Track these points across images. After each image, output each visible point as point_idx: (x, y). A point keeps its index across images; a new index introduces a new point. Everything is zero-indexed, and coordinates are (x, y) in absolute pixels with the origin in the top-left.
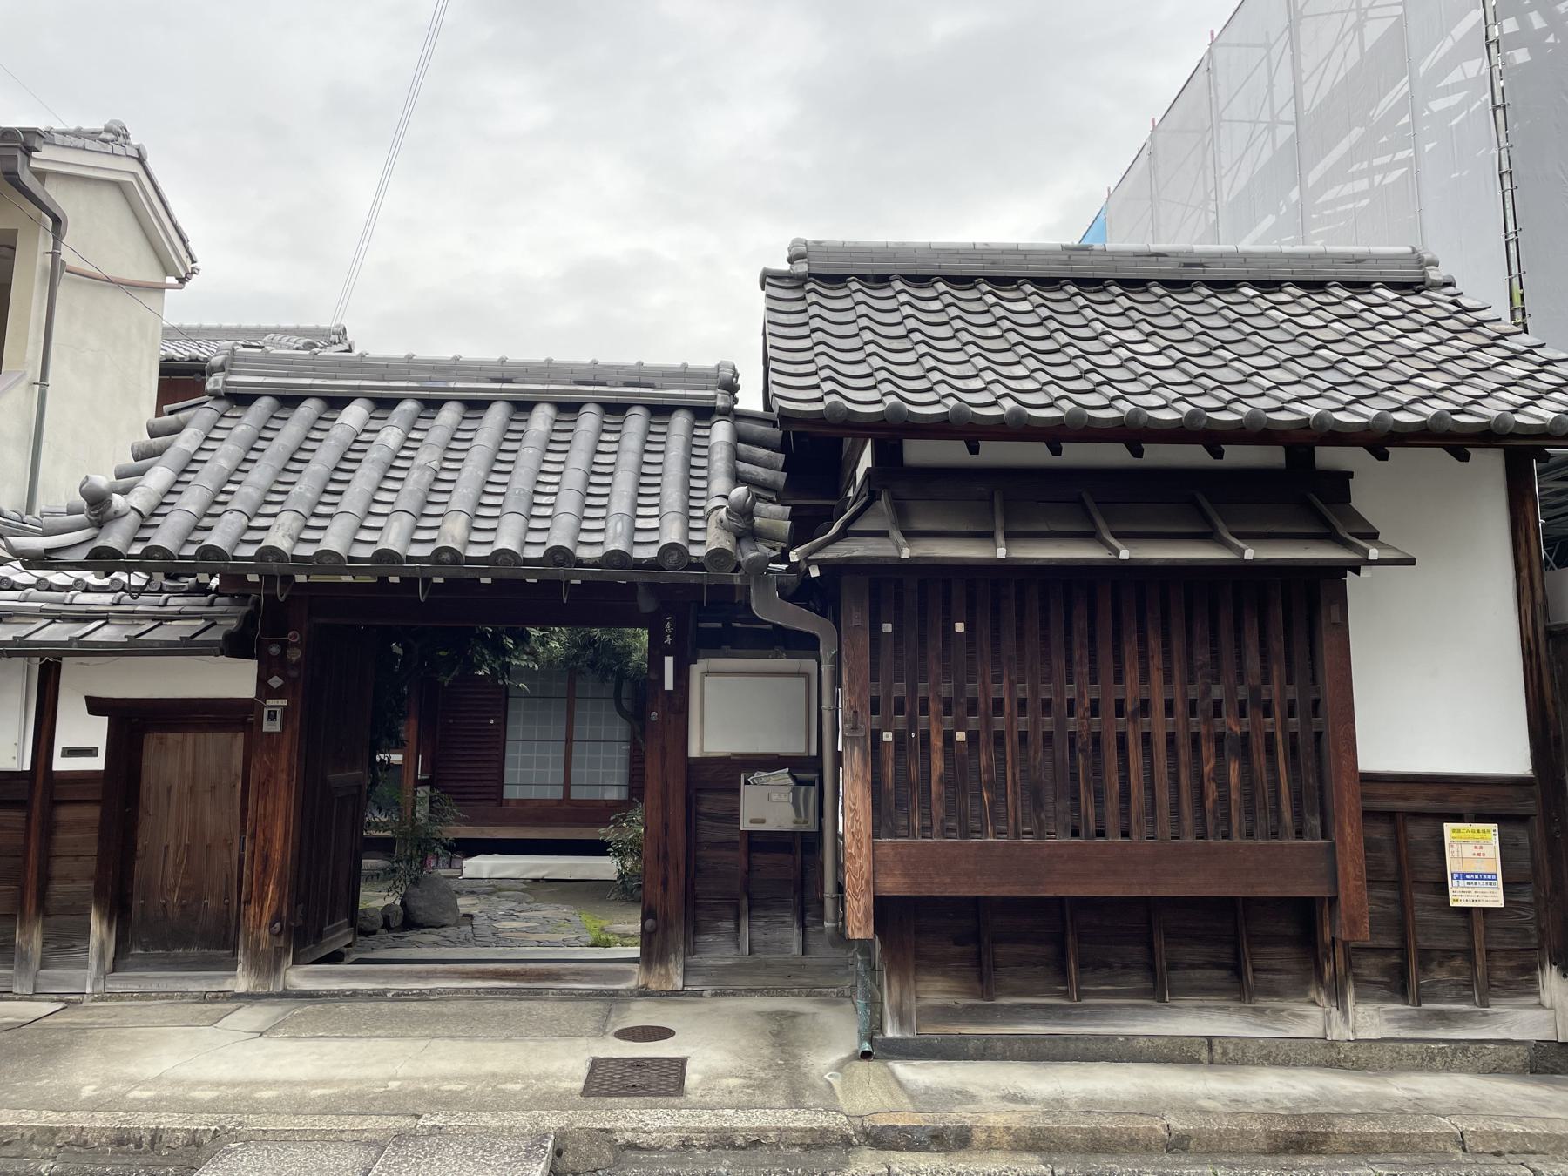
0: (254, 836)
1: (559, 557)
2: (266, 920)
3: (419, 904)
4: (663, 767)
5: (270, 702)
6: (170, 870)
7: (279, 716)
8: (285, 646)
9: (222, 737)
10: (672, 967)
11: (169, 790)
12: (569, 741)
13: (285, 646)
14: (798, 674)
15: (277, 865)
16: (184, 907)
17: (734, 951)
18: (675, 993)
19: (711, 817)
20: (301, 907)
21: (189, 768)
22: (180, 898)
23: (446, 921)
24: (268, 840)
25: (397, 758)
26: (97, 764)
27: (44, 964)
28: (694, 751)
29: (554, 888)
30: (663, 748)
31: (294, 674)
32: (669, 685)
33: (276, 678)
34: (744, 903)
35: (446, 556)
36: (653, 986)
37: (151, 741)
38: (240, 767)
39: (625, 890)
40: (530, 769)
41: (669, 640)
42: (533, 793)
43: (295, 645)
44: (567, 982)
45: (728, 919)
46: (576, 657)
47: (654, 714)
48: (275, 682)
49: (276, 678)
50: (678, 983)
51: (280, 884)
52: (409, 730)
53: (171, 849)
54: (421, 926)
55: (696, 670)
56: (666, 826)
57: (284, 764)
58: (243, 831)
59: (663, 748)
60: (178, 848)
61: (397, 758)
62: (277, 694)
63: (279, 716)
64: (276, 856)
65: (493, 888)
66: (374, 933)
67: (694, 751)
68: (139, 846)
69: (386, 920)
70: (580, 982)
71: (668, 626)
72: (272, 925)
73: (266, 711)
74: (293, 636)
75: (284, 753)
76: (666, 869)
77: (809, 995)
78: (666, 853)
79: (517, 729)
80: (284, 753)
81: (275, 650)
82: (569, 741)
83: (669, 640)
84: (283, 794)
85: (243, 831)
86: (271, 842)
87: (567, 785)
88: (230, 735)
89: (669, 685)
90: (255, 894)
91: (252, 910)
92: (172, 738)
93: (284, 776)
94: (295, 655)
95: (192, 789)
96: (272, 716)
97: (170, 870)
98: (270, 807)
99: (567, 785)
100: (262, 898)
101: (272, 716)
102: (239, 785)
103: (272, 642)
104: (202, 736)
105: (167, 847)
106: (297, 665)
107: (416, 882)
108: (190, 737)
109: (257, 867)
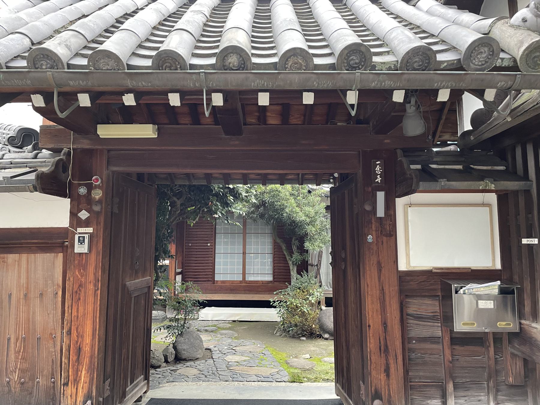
0: (69, 332)
1: (355, 59)
3: (185, 348)
4: (379, 278)
5: (80, 230)
6: (12, 356)
7: (86, 241)
8: (90, 188)
11: (10, 296)
12: (244, 253)
13: (90, 188)
14: (483, 205)
15: (88, 355)
16: (22, 384)
19: (419, 318)
20: (107, 382)
21: (23, 280)
22: (20, 378)
23: (198, 356)
24: (80, 336)
25: (167, 262)
27: (397, 61)
28: (402, 266)
29: (246, 326)
31: (97, 208)
32: (381, 212)
34: (450, 387)
35: (233, 60)
38: (61, 279)
39: (285, 330)
40: (227, 265)
41: (379, 179)
42: (228, 278)
43: (98, 187)
45: (435, 398)
46: (253, 212)
48: (84, 215)
51: (90, 369)
52: (172, 248)
53: (13, 340)
54: (185, 360)
55: (400, 202)
56: (385, 324)
57: (91, 277)
58: (63, 328)
60: (17, 340)
61: (167, 262)
62: (86, 223)
63: (86, 241)
64: (86, 349)
65: (215, 328)
66: (159, 367)
67: (402, 266)
69: (166, 357)
73: (77, 237)
74: (97, 181)
75: (91, 269)
78: (386, 346)
79: (220, 248)
80: (91, 269)
81: (83, 191)
82: (244, 253)
83: (379, 179)
84: (91, 299)
85: (63, 328)
86: (82, 337)
87: (244, 274)
89: (381, 212)
91: (70, 390)
92: (11, 257)
93: (91, 287)
94: (97, 194)
95: (26, 295)
96: (82, 241)
97: (12, 356)
98: (81, 309)
99: (244, 274)
100: (76, 381)
101: (82, 241)
102: (60, 293)
103: (80, 185)
105: (9, 339)
106: (100, 201)
107: (181, 335)
108: (24, 256)
109: (73, 357)
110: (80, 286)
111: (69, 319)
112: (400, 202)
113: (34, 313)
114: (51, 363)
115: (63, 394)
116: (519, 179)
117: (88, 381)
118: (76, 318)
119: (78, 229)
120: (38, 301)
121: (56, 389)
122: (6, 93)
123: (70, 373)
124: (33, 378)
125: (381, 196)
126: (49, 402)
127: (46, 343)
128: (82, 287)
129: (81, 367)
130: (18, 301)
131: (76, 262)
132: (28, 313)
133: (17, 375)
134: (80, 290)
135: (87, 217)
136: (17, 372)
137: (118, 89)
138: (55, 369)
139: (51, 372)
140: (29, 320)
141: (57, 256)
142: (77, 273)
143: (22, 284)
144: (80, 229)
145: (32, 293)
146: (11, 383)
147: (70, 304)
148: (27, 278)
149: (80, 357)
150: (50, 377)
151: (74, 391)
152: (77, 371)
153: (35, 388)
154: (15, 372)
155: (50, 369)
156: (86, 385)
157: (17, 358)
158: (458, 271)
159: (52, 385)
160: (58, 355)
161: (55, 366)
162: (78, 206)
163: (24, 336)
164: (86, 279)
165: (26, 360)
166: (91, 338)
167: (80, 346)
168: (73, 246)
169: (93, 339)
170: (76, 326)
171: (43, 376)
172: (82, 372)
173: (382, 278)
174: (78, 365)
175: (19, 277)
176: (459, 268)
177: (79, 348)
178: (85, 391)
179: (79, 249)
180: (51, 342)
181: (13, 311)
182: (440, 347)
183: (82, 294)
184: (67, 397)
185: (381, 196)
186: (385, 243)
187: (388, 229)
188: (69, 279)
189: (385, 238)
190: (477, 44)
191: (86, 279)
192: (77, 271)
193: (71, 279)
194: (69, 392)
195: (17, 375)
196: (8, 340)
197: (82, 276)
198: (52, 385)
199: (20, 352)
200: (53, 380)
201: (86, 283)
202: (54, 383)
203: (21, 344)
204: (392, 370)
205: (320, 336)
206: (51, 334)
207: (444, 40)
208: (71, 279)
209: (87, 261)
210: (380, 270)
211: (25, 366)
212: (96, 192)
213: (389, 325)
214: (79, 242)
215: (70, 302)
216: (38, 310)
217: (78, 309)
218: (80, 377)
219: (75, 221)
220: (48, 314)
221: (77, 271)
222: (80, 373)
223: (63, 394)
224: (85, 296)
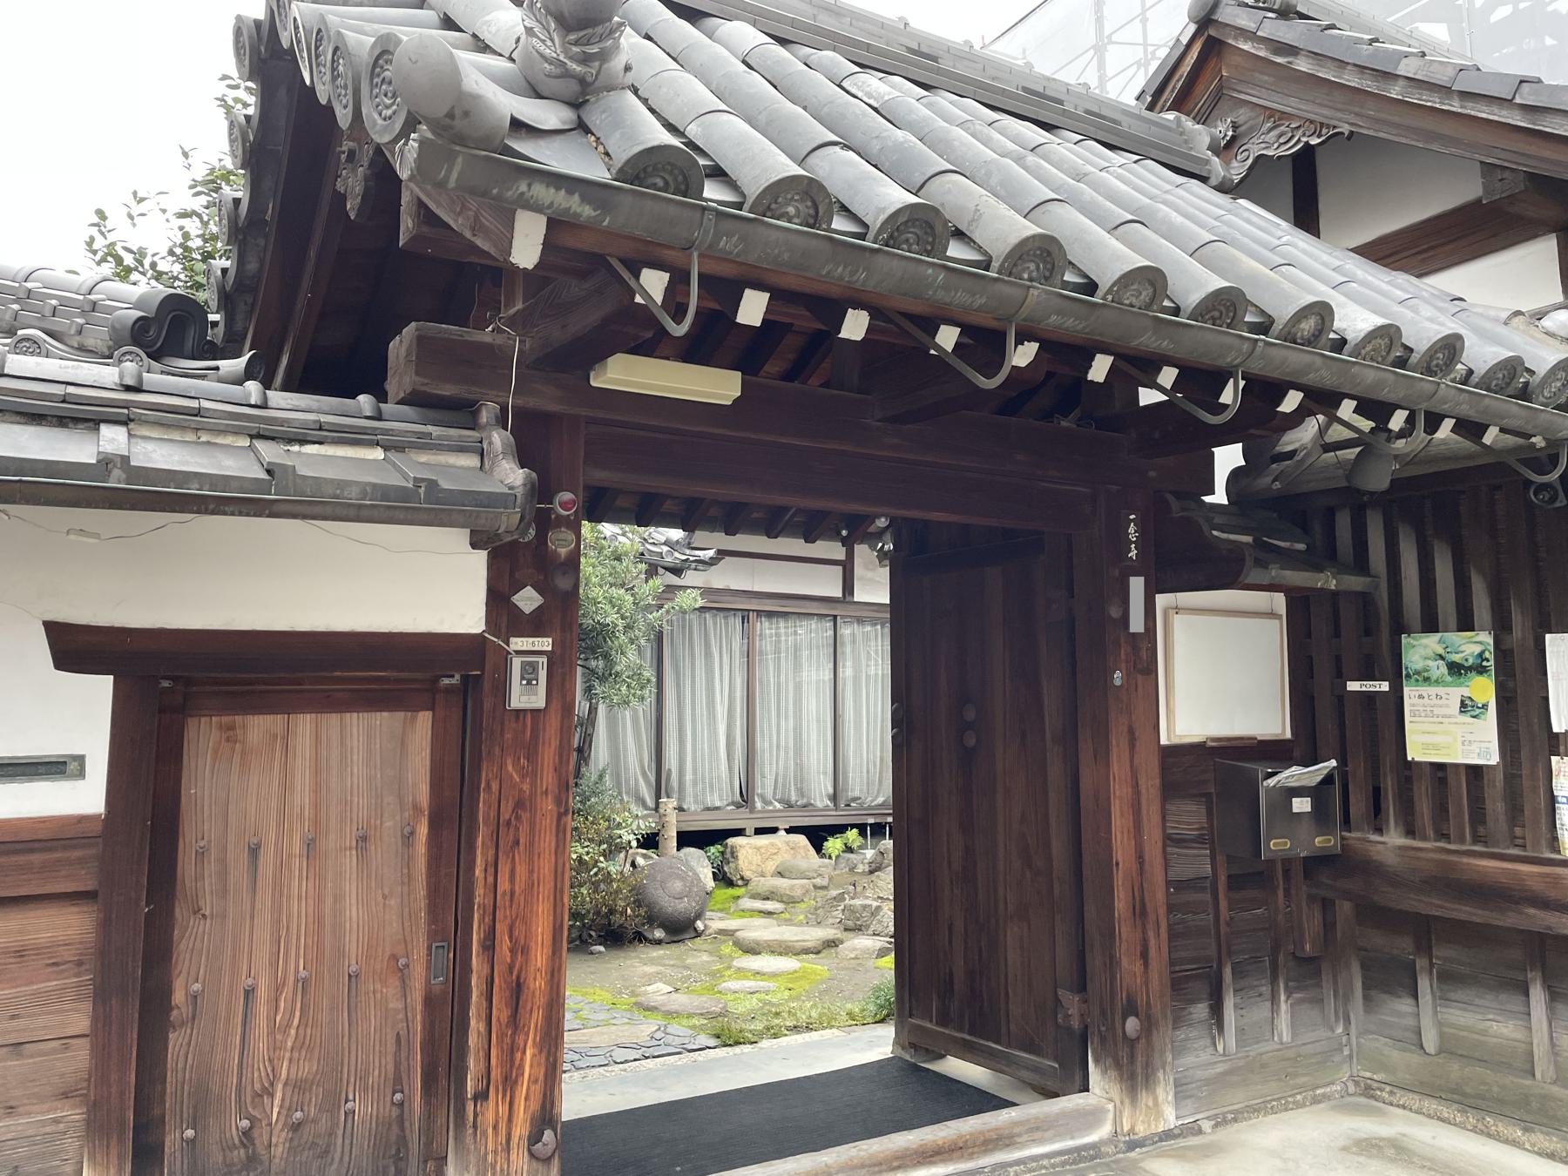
2: (521, 1129)
5: (518, 643)
9: (383, 722)
10: (1160, 1091)
11: (254, 852)
16: (296, 1127)
17: (1210, 1050)
18: (1168, 1135)
24: (521, 949)
26: (87, 797)
30: (1131, 731)
33: (529, 592)
36: (1142, 1130)
37: (203, 738)
41: (1133, 554)
44: (1023, 1146)
45: (1199, 1000)
47: (1118, 674)
48: (528, 600)
49: (529, 592)
50: (1170, 1118)
53: (262, 993)
56: (1140, 858)
59: (1131, 731)
60: (278, 989)
68: (178, 997)
70: (1041, 1141)
71: (1132, 528)
72: (535, 1138)
73: (517, 663)
76: (1144, 932)
77: (1316, 1101)
83: (1133, 554)
86: (525, 950)
88: (400, 715)
89: (1137, 624)
90: (496, 1074)
91: (492, 1110)
92: (259, 726)
95: (310, 845)
97: (261, 1045)
98: (521, 870)
100: (510, 1082)
104: (334, 719)
105: (249, 993)
108: (304, 723)
109: (501, 1012)
110: (519, 804)
111: (489, 901)
112: (1161, 600)
113: (338, 898)
114: (391, 1048)
115: (475, 1126)
116: (1342, 569)
117: (541, 1077)
118: (508, 898)
119: (513, 640)
120: (350, 861)
121: (407, 1124)
122: (1068, 345)
123: (493, 1061)
124: (333, 1102)
125: (1137, 585)
126: (385, 1168)
127: (378, 986)
128: (524, 809)
129: (522, 1037)
130: (282, 865)
131: (508, 736)
132: (320, 900)
133: (277, 1102)
134: (518, 818)
135: (536, 605)
136: (279, 1095)
137: (835, 292)
138: (404, 1063)
139: (391, 1075)
140: (319, 921)
141: (414, 719)
142: (510, 768)
143: (297, 810)
144: (519, 640)
145: (332, 836)
146: (256, 1133)
147: (491, 858)
148: (317, 789)
149: (521, 1010)
150: (389, 1091)
151: (503, 1110)
152: (512, 1053)
153: (340, 1132)
154: (272, 1096)
155: (391, 1067)
156: (537, 1089)
157: (275, 1047)
158: (1234, 743)
159: (395, 1112)
160: (414, 1017)
161: (404, 1055)
162: (512, 574)
163: (303, 974)
164: (533, 784)
165: (310, 1050)
166: (548, 951)
167: (518, 978)
168: (502, 689)
169: (554, 953)
170: (508, 921)
171: (366, 1090)
172: (524, 1052)
173: (1136, 761)
174: (514, 1033)
175: (286, 787)
176: (1241, 738)
177: (519, 985)
178: (535, 1105)
179: (524, 699)
180: (394, 982)
181: (265, 897)
182: (1208, 897)
183: (524, 829)
184: (484, 1133)
185: (1137, 585)
186: (1140, 689)
187: (1143, 657)
188: (488, 786)
189: (1140, 677)
190: (902, 219)
191: (533, 784)
192: (509, 762)
193: (495, 786)
194: (490, 1116)
195: (277, 1102)
196: (247, 993)
197: (523, 777)
198: (395, 1112)
199: (289, 1026)
200: (398, 1096)
201: (533, 794)
202: (401, 1104)
203: (294, 1001)
204: (1153, 952)
205: (640, 938)
206: (394, 958)
207: (963, 228)
208: (495, 786)
209: (535, 730)
210: (1132, 747)
211: (307, 1069)
212: (562, 536)
213: (1147, 858)
214: (522, 678)
215: (492, 852)
216: (350, 888)
217: (513, 871)
218: (521, 1067)
219: (505, 619)
220: (385, 897)
221: (509, 762)
222: (518, 1055)
223: (475, 1126)
224: (532, 829)
